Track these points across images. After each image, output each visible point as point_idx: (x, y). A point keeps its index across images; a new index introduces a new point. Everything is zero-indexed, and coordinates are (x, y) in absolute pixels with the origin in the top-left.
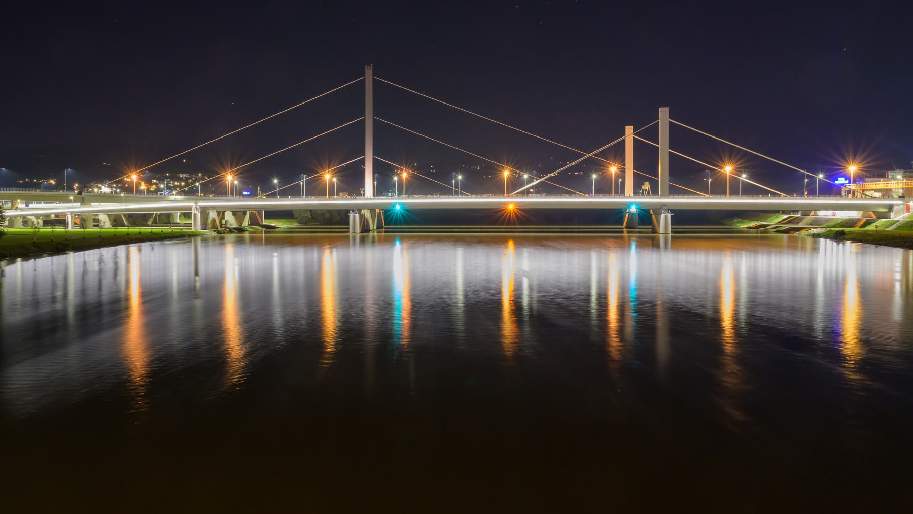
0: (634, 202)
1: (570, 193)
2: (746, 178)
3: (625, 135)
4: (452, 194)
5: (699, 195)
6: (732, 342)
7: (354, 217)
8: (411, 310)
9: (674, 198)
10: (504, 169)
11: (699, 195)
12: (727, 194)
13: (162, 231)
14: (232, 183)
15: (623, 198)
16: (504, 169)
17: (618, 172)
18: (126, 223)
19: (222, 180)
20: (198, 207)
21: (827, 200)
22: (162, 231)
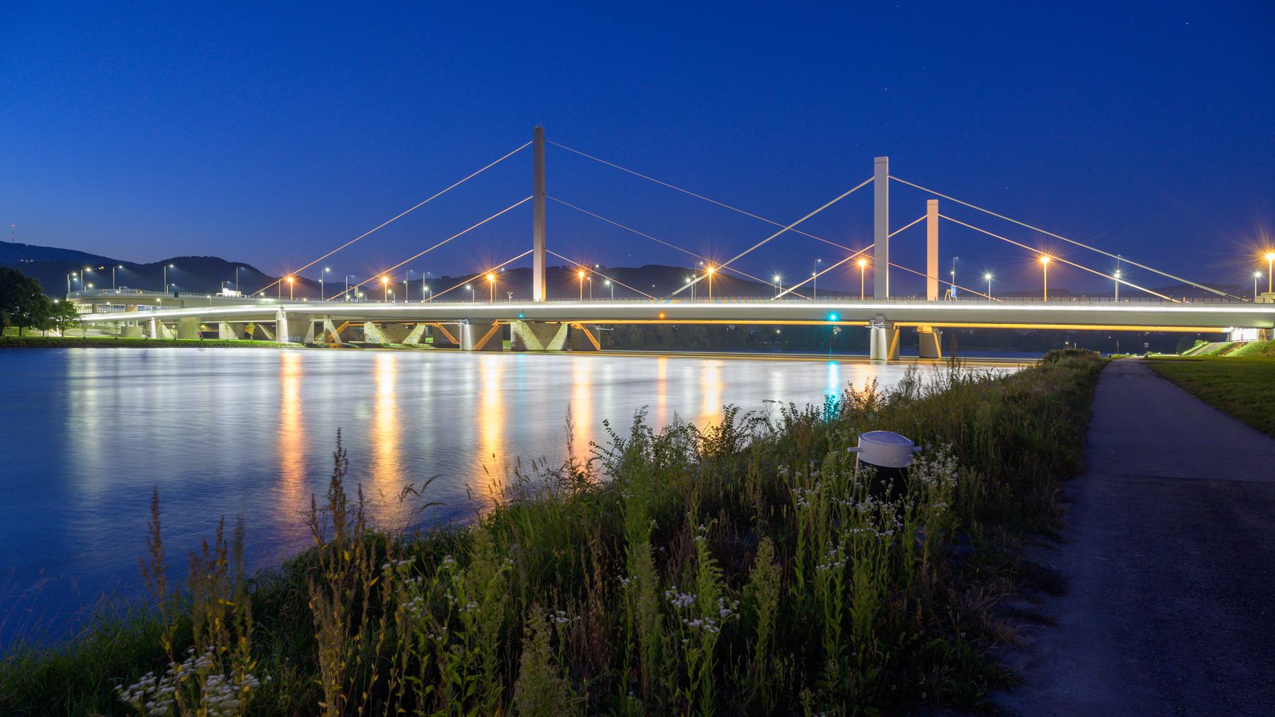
0: (834, 309)
1: (641, 297)
2: (1120, 279)
3: (926, 214)
4: (1042, 299)
5: (1162, 299)
6: (177, 382)
7: (877, 333)
8: (282, 412)
9: (729, 303)
10: (577, 268)
11: (1162, 299)
12: (861, 296)
13: (116, 339)
14: (585, 280)
15: (924, 304)
16: (577, 268)
17: (1051, 262)
18: (598, 345)
19: (847, 269)
20: (285, 313)
21: (966, 304)
22: (116, 339)
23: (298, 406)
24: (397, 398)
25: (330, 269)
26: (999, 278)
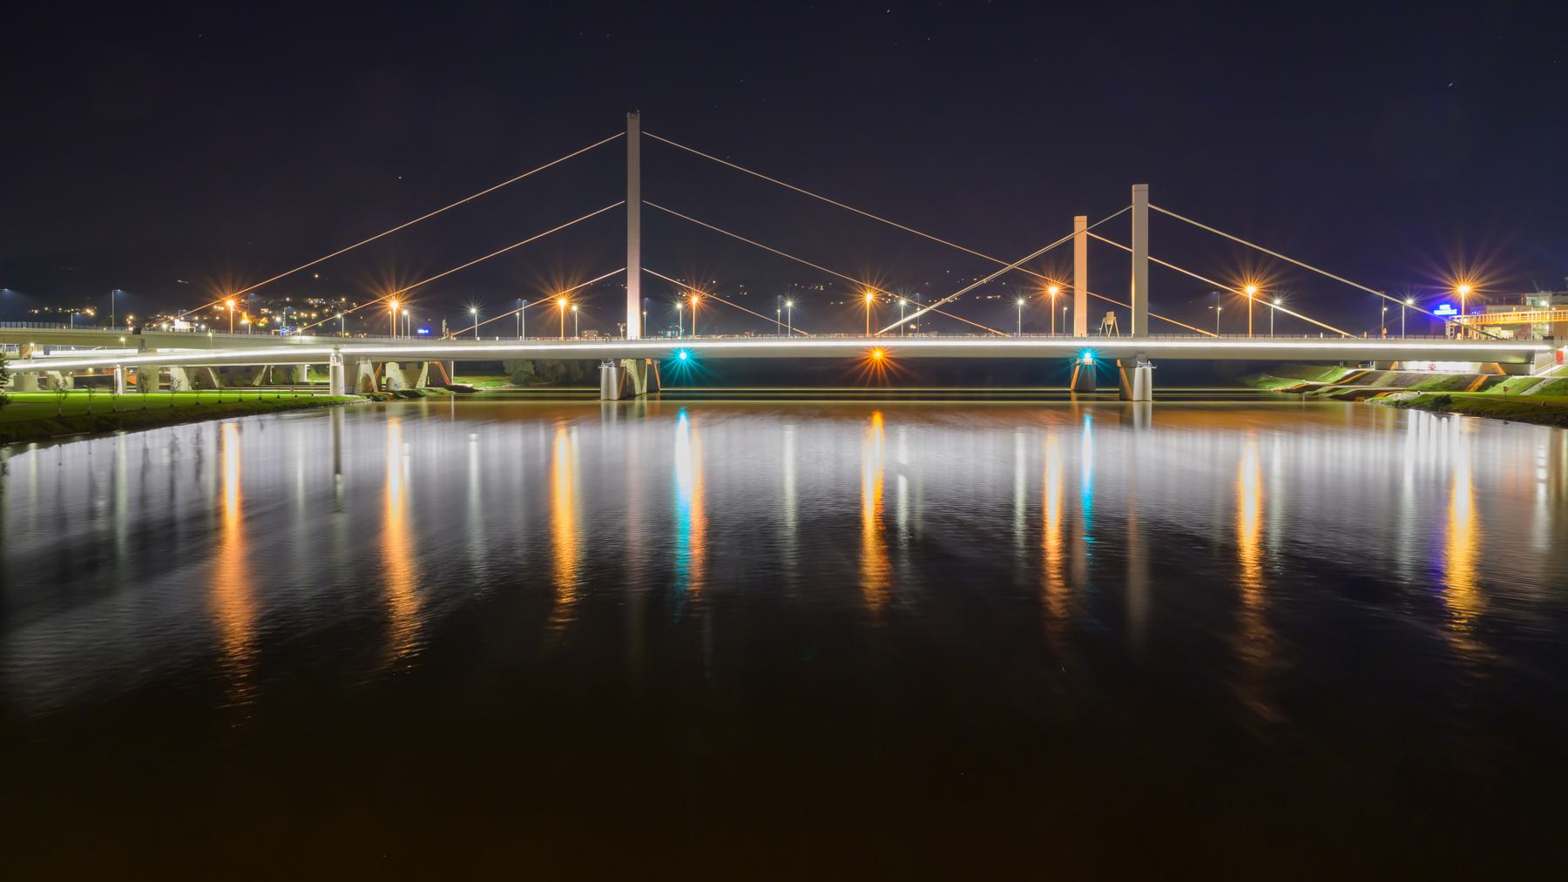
0: (1089, 347)
1: (979, 332)
2: (1281, 306)
3: (1073, 231)
4: (777, 333)
5: (1201, 334)
7: (608, 372)
9: (1157, 340)
11: (1201, 334)
12: (1248, 333)
13: (278, 397)
14: (399, 314)
15: (1070, 340)
17: (1062, 295)
18: (216, 382)
20: (341, 355)
21: (1420, 343)
22: (278, 397)
23: (970, 490)
24: (1474, 492)
25: (791, 300)
26: (801, 305)
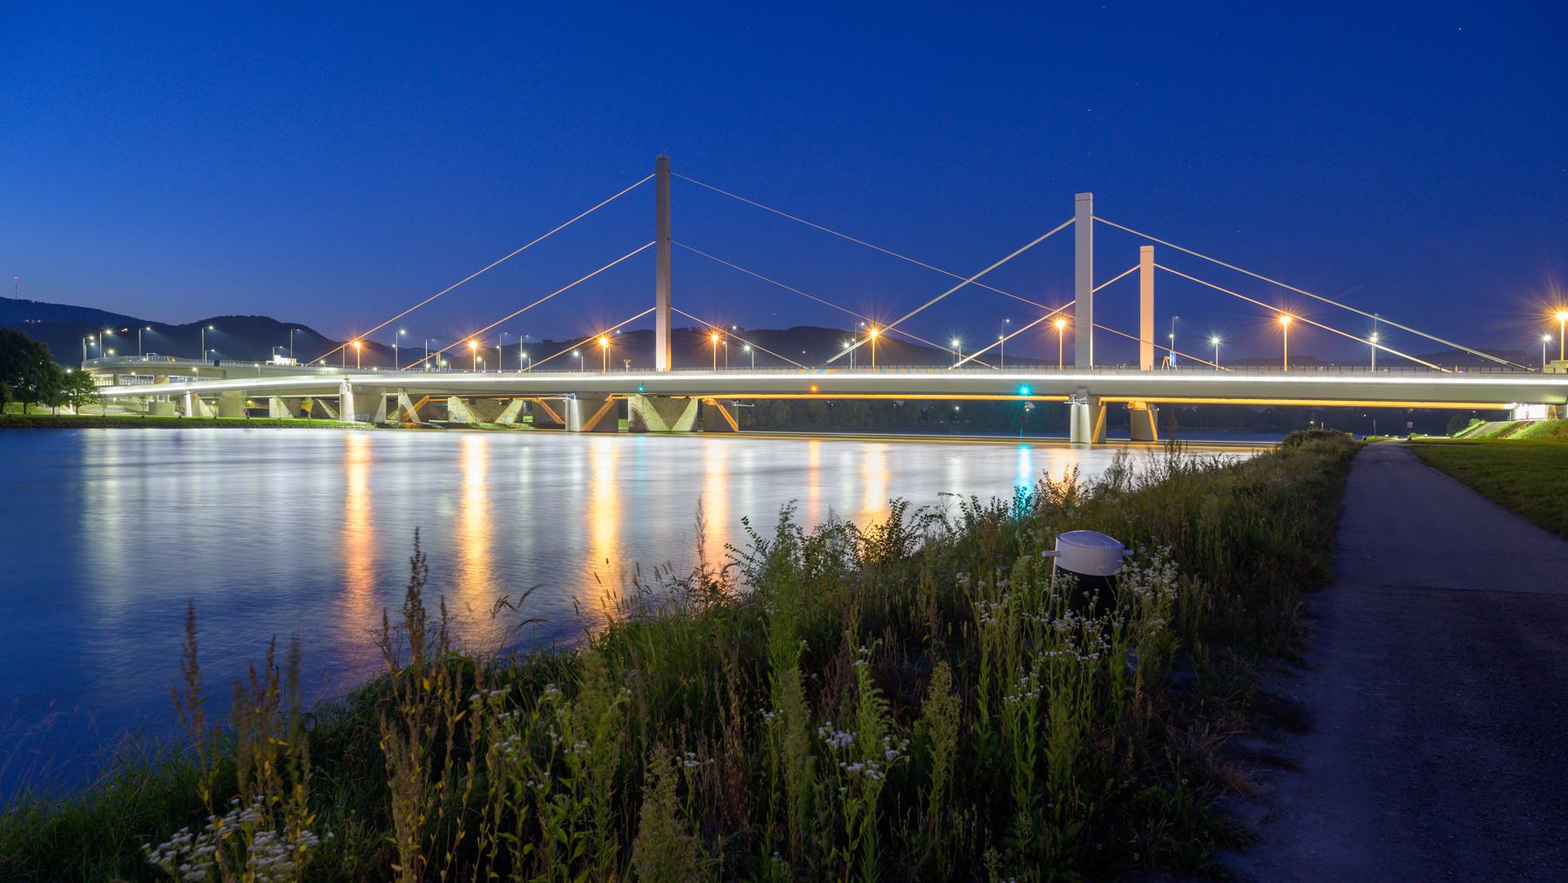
0: (1025, 381)
1: (788, 366)
2: (1377, 343)
3: (1139, 263)
4: (1282, 369)
5: (1428, 369)
7: (1079, 410)
8: (347, 507)
9: (897, 373)
10: (709, 330)
11: (1428, 369)
12: (1059, 364)
13: (143, 417)
14: (719, 345)
15: (1137, 374)
16: (709, 330)
17: (1293, 323)
18: (735, 425)
19: (1041, 332)
20: (350, 385)
21: (1188, 375)
22: (143, 417)
23: (367, 499)
24: (489, 490)
25: (406, 331)
26: (1229, 343)
